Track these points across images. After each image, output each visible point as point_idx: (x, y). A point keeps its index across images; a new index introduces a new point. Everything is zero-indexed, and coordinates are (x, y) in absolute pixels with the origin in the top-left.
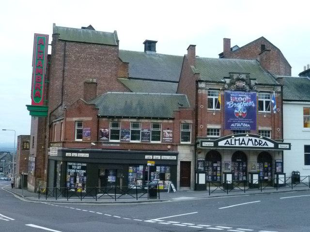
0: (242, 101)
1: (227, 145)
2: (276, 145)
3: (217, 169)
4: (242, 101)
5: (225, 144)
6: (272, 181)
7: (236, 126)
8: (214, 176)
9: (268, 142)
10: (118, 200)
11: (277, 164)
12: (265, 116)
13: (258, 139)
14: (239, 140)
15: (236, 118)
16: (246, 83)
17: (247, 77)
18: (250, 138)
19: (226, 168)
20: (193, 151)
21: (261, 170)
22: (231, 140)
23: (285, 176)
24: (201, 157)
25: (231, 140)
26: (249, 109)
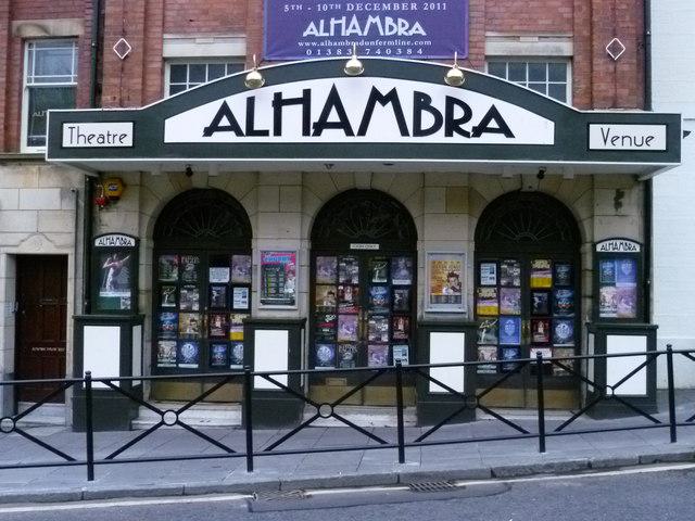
1: (218, 137)
2: (572, 130)
5: (208, 132)
9: (510, 112)
10: (105, 479)
11: (607, 267)
13: (438, 94)
14: (305, 100)
18: (385, 85)
23: (652, 343)
24: (122, 226)
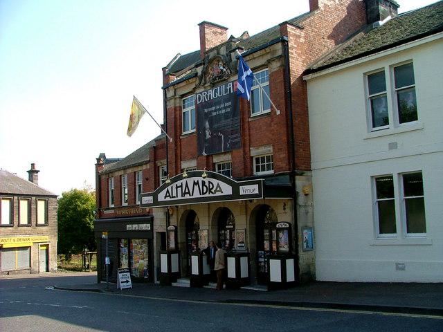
13: (200, 179)
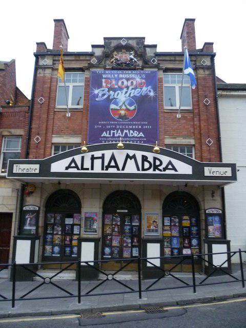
0: (127, 87)
1: (70, 170)
3: (72, 229)
4: (127, 87)
5: (67, 168)
6: (201, 258)
7: (114, 136)
8: (66, 246)
11: (210, 219)
12: (179, 116)
13: (150, 156)
14: (103, 158)
15: (114, 120)
16: (136, 53)
17: (138, 44)
19: (89, 228)
20: (18, 190)
21: (175, 233)
22: (83, 158)
24: (33, 203)
25: (83, 158)
26: (141, 101)
